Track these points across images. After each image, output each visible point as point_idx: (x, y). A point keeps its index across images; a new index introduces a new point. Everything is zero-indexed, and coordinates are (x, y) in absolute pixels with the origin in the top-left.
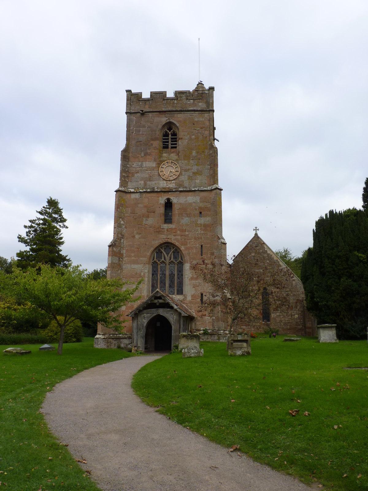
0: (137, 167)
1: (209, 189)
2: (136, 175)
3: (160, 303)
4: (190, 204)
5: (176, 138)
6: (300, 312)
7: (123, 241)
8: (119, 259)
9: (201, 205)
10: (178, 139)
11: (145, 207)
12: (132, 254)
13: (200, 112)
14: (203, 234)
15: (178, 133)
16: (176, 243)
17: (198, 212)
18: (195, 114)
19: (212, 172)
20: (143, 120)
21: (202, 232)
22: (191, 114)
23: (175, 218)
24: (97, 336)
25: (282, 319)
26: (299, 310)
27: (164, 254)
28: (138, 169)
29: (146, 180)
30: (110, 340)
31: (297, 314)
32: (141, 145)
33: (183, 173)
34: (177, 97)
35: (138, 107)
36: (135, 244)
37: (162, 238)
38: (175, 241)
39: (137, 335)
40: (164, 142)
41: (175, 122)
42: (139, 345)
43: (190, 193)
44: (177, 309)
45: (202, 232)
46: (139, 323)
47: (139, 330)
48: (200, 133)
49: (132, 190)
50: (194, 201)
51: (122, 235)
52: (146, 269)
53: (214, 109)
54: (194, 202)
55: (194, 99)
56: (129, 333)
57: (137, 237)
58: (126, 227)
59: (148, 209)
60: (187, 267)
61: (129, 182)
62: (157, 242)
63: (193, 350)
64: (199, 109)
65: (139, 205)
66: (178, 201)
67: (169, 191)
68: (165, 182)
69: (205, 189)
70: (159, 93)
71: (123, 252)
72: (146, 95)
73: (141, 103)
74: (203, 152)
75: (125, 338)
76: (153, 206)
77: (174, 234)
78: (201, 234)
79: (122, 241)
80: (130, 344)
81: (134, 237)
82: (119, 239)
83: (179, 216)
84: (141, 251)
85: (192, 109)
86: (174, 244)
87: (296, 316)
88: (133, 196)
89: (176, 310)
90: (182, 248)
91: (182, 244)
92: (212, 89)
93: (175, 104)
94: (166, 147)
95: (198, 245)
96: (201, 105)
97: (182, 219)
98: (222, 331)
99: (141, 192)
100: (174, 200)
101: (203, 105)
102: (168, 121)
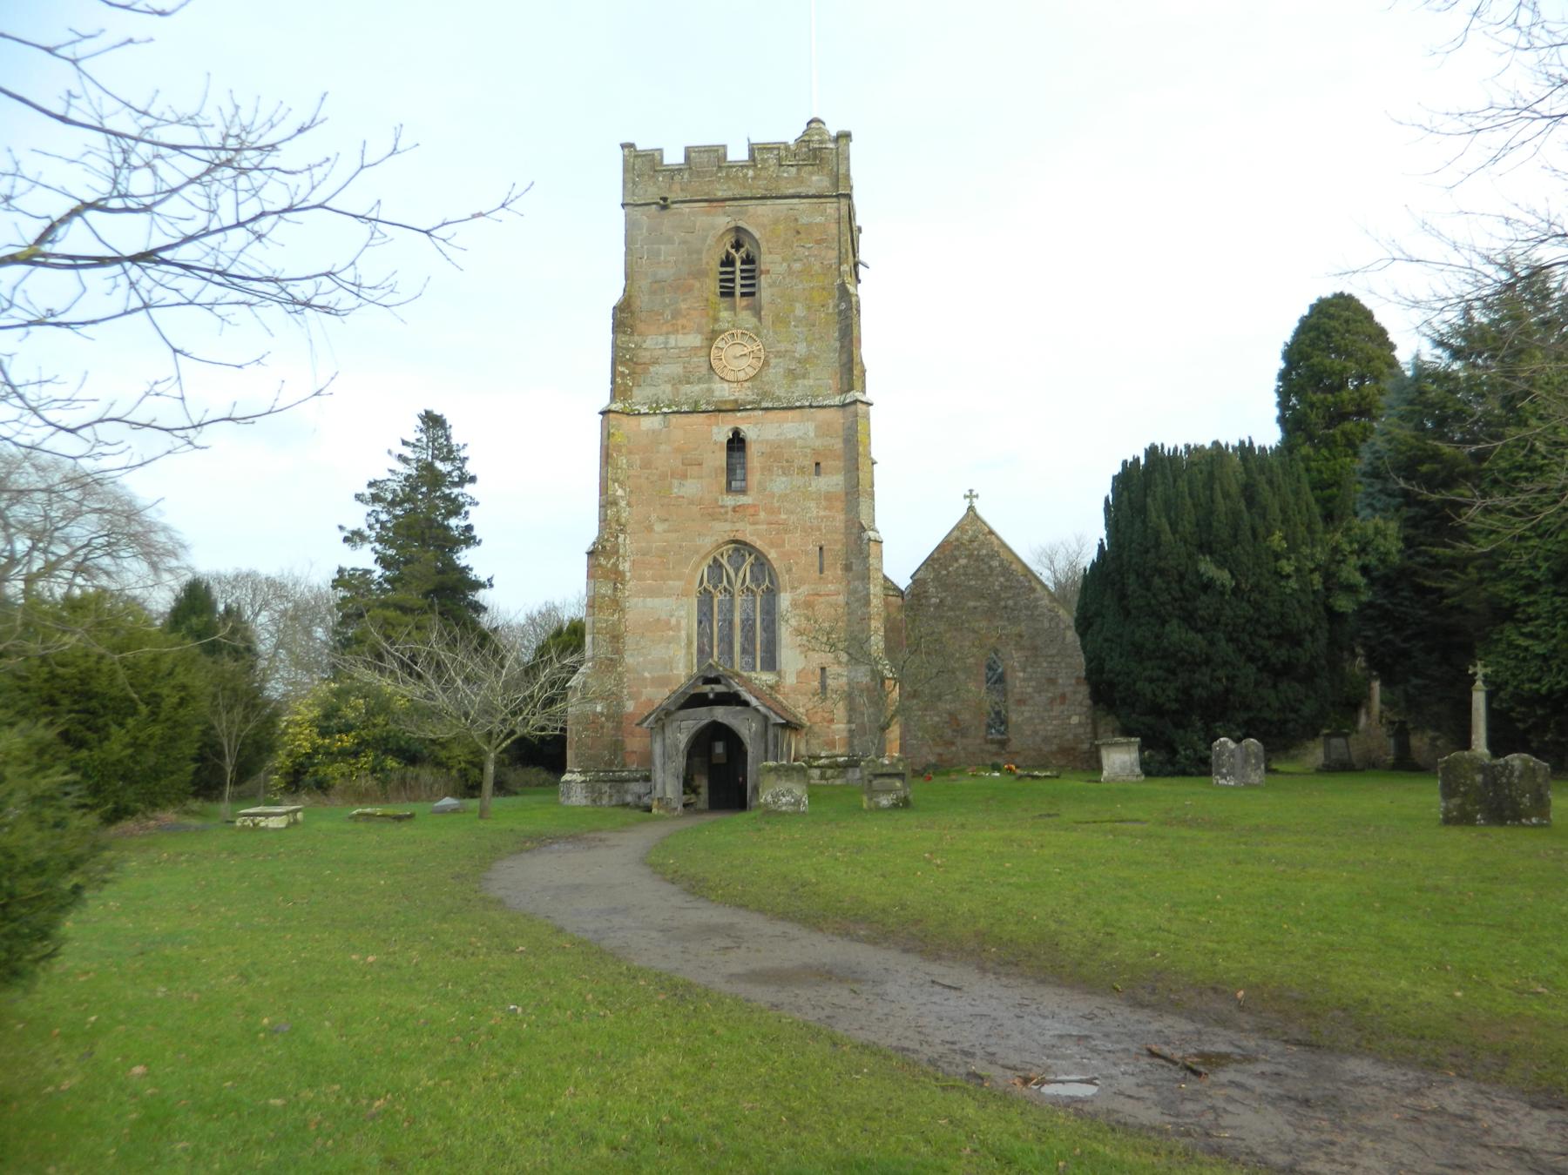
2: (651, 369)
3: (718, 695)
9: (818, 443)
11: (678, 450)
13: (815, 200)
17: (809, 463)
19: (845, 357)
21: (822, 513)
24: (567, 777)
26: (1080, 704)
28: (657, 353)
29: (677, 381)
30: (598, 785)
32: (663, 288)
33: (773, 361)
38: (754, 538)
40: (721, 280)
41: (750, 229)
43: (790, 414)
46: (668, 741)
49: (644, 410)
50: (801, 433)
54: (800, 437)
57: (658, 527)
58: (629, 504)
65: (663, 447)
67: (737, 407)
68: (726, 385)
72: (673, 157)
75: (636, 780)
81: (650, 529)
85: (791, 191)
87: (1075, 720)
88: (648, 423)
90: (772, 555)
91: (772, 545)
92: (845, 136)
94: (727, 293)
100: (750, 432)
102: (732, 224)
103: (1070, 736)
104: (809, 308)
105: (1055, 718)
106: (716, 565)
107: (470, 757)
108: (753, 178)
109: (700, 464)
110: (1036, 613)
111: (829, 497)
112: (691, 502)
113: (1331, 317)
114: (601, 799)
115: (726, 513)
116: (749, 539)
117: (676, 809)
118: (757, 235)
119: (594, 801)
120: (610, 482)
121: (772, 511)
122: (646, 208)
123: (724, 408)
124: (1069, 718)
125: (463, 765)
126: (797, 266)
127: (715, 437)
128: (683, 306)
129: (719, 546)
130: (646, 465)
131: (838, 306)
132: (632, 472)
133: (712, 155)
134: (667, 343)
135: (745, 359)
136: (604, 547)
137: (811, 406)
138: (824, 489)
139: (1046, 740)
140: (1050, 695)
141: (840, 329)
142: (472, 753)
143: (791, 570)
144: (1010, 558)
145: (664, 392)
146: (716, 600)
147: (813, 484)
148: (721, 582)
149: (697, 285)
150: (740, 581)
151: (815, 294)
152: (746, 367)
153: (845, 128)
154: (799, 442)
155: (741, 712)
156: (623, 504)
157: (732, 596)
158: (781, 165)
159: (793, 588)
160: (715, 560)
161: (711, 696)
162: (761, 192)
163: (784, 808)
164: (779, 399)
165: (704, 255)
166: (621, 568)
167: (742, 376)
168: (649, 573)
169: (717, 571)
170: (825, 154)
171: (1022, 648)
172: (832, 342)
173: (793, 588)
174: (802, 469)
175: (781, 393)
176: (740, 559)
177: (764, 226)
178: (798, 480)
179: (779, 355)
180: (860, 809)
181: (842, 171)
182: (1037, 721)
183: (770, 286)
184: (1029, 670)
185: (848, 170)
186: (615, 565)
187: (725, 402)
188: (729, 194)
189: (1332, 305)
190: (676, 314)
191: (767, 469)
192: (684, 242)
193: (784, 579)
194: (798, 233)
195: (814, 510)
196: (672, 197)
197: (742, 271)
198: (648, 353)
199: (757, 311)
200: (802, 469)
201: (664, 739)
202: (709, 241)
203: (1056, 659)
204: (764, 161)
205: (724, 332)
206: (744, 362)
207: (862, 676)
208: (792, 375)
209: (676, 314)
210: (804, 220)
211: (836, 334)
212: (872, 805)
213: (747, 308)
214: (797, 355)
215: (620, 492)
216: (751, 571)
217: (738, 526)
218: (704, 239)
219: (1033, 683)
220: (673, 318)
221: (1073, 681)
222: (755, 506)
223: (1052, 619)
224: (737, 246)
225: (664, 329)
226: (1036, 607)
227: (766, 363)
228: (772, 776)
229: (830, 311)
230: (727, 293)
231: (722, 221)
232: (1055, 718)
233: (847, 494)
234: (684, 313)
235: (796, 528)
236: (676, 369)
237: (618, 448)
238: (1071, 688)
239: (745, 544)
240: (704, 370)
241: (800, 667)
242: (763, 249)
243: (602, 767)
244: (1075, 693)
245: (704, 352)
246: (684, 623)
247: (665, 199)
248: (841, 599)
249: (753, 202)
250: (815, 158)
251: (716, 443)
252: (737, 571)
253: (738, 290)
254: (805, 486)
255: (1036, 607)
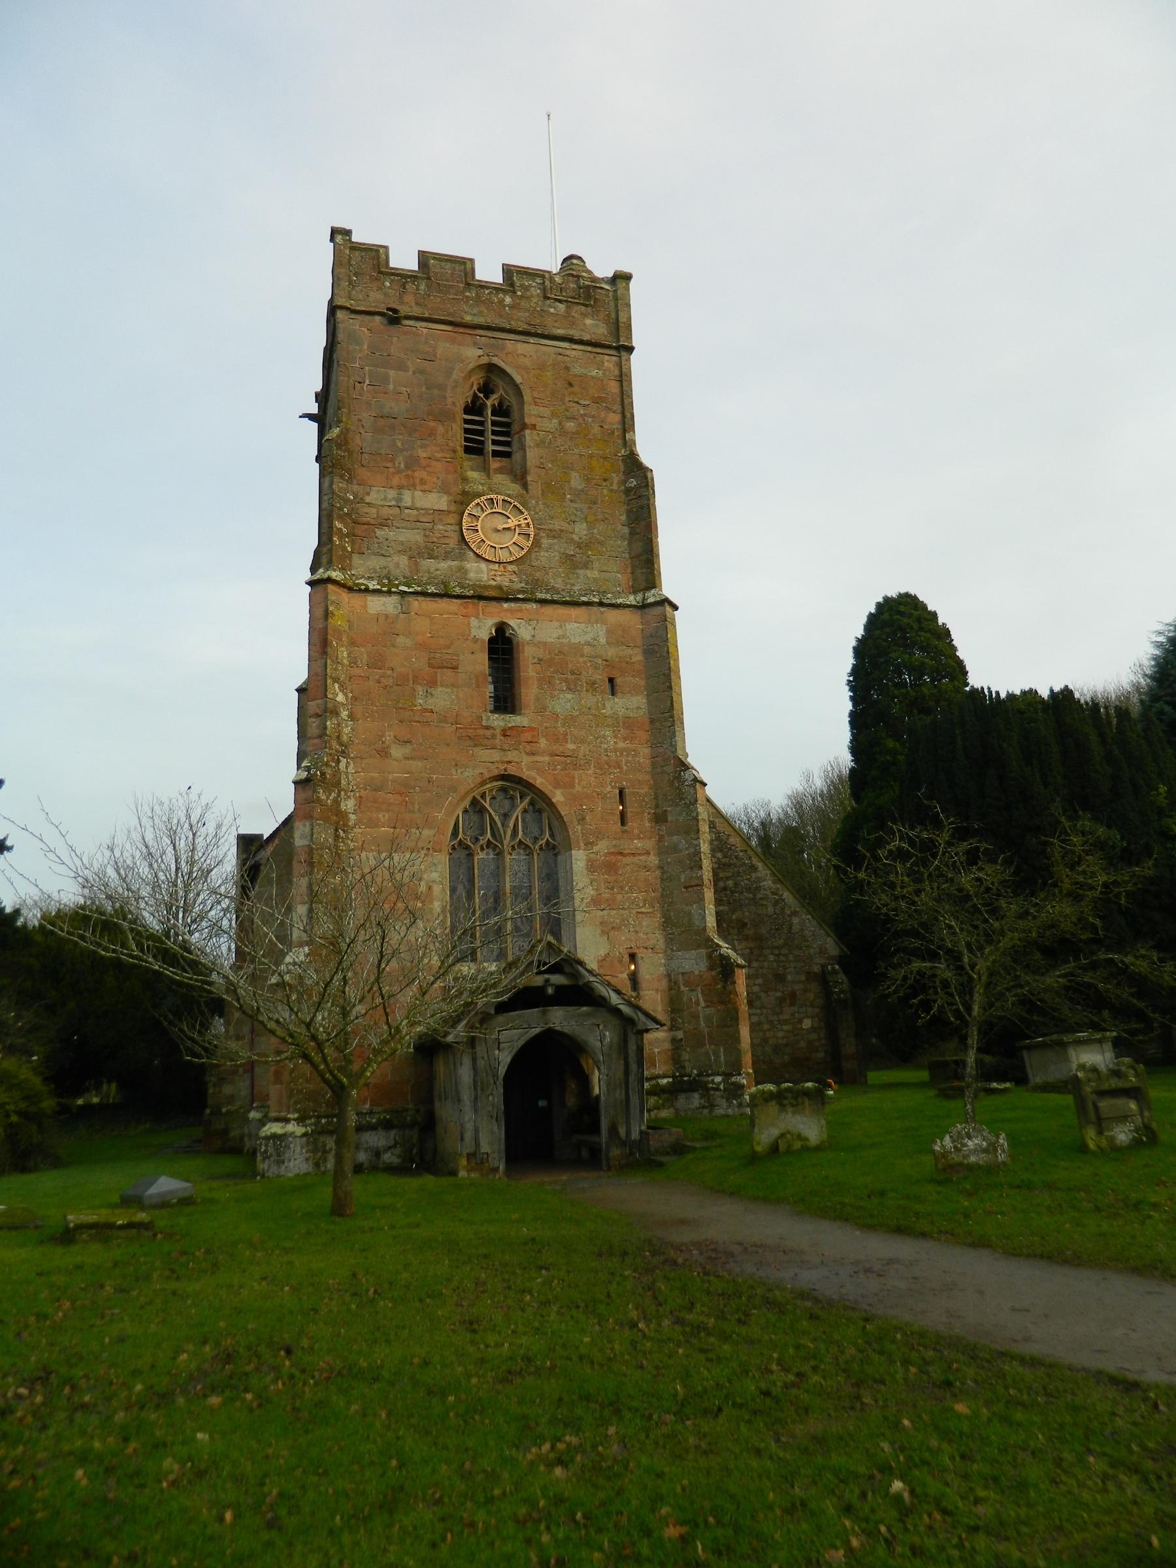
0: (382, 503)
1: (634, 603)
2: (379, 533)
3: (559, 988)
4: (577, 649)
5: (508, 425)
6: (817, 1010)
7: (347, 767)
8: (336, 830)
9: (611, 653)
10: (516, 427)
11: (421, 646)
12: (380, 816)
13: (589, 349)
14: (622, 751)
15: (515, 407)
16: (535, 779)
17: (600, 677)
18: (574, 352)
19: (638, 547)
20: (397, 341)
21: (621, 745)
22: (560, 351)
23: (529, 692)
25: (768, 1034)
26: (812, 1005)
27: (490, 814)
28: (385, 512)
29: (416, 554)
30: (322, 1139)
31: (808, 1017)
32: (392, 427)
33: (545, 542)
34: (512, 285)
35: (379, 296)
36: (391, 776)
37: (488, 760)
38: (533, 774)
39: (476, 1111)
40: (467, 431)
41: (509, 370)
42: (485, 1148)
43: (574, 612)
44: (620, 1006)
45: (621, 745)
46: (481, 1063)
47: (482, 1090)
48: (593, 417)
49: (373, 585)
50: (588, 637)
51: (341, 744)
52: (433, 868)
53: (635, 342)
54: (588, 644)
55: (566, 301)
56: (380, 1109)
57: (397, 752)
58: (352, 717)
59: (432, 655)
60: (579, 858)
61: (355, 558)
62: (469, 773)
63: (970, 1138)
64: (586, 337)
65: (400, 640)
66: (534, 636)
67: (503, 597)
68: (483, 565)
69: (620, 601)
70: (450, 261)
71: (346, 806)
72: (404, 259)
73: (388, 284)
74: (605, 480)
76: (448, 647)
77: (528, 748)
78: (616, 750)
79: (342, 765)
80: (390, 1148)
81: (384, 753)
82: (333, 760)
83: (540, 687)
84: (413, 804)
85: (560, 332)
86: (531, 784)
87: (807, 1024)
88: (376, 605)
89: (616, 1011)
90: (558, 797)
91: (557, 785)
92: (622, 278)
93: (504, 306)
94: (474, 448)
95: (609, 789)
96: (593, 326)
97: (553, 697)
98: (718, 1079)
99: (405, 592)
100: (522, 629)
101: (597, 325)
102: (485, 360)
103: (803, 1044)
104: (588, 480)
105: (786, 1022)
106: (476, 807)
107: (23, 1105)
108: (512, 307)
109: (455, 668)
110: (759, 896)
111: (629, 724)
112: (444, 719)
113: (902, 614)
114: (325, 1160)
115: (494, 737)
116: (527, 774)
117: (496, 1170)
118: (518, 379)
119: (317, 1165)
120: (329, 681)
121: (557, 739)
122: (367, 318)
123: (486, 594)
124: (800, 1021)
125: (14, 1118)
126: (570, 426)
127: (474, 632)
128: (422, 454)
129: (483, 783)
130: (377, 662)
131: (625, 482)
132: (357, 671)
133: (457, 267)
134: (399, 500)
135: (508, 534)
136: (323, 774)
137: (601, 604)
138: (622, 712)
139: (776, 1049)
140: (779, 994)
141: (629, 512)
142: (25, 1098)
143: (583, 819)
144: (728, 831)
145: (397, 565)
146: (476, 858)
147: (608, 705)
148: (483, 833)
149: (441, 429)
150: (509, 832)
151: (594, 463)
152: (510, 546)
153: (625, 268)
154: (587, 649)
155: (589, 1015)
156: (344, 714)
157: (499, 854)
158: (546, 298)
159: (589, 845)
160: (474, 802)
161: (550, 991)
162: (522, 327)
163: (973, 1159)
164: (554, 590)
165: (449, 393)
166: (343, 808)
167: (504, 556)
168: (383, 817)
169: (475, 818)
170: (599, 294)
171: (746, 938)
172: (620, 527)
173: (589, 845)
174: (592, 685)
175: (558, 583)
176: (507, 803)
177: (526, 369)
178: (589, 700)
179: (555, 534)
180: (1083, 1149)
181: (622, 319)
182: (766, 1027)
183: (537, 445)
184: (755, 964)
185: (629, 318)
186: (337, 802)
187: (486, 587)
188: (481, 320)
189: (900, 604)
190: (412, 463)
191: (546, 682)
192: (422, 372)
193: (576, 830)
194: (571, 385)
195: (611, 740)
196: (404, 310)
197: (494, 423)
198: (374, 510)
199: (521, 477)
200: (592, 685)
201: (474, 1060)
202: (454, 376)
203: (784, 951)
204: (527, 288)
205: (479, 495)
206: (508, 540)
207: (693, 963)
208: (571, 563)
209: (412, 463)
210: (577, 370)
211: (623, 518)
212: (1104, 1143)
213: (500, 471)
214: (576, 538)
215: (340, 698)
216: (523, 821)
217: (512, 756)
218: (449, 373)
219: (760, 981)
220: (408, 467)
221: (803, 978)
222: (531, 729)
223: (776, 903)
224: (487, 389)
225: (395, 481)
226: (758, 888)
227: (537, 543)
228: (773, 1107)
229: (615, 487)
230: (474, 448)
231: (472, 353)
232: (786, 1022)
233: (652, 721)
234: (423, 462)
235: (588, 763)
236: (414, 537)
237: (339, 633)
238: (801, 986)
239: (518, 781)
240: (453, 541)
241: (602, 952)
242: (527, 397)
243: (323, 1109)
244: (805, 991)
245: (452, 519)
246: (437, 889)
247: (395, 311)
248: (653, 860)
249: (512, 336)
250: (588, 297)
251: (475, 640)
252: (506, 816)
253: (490, 447)
254: (597, 708)
255: (758, 888)
